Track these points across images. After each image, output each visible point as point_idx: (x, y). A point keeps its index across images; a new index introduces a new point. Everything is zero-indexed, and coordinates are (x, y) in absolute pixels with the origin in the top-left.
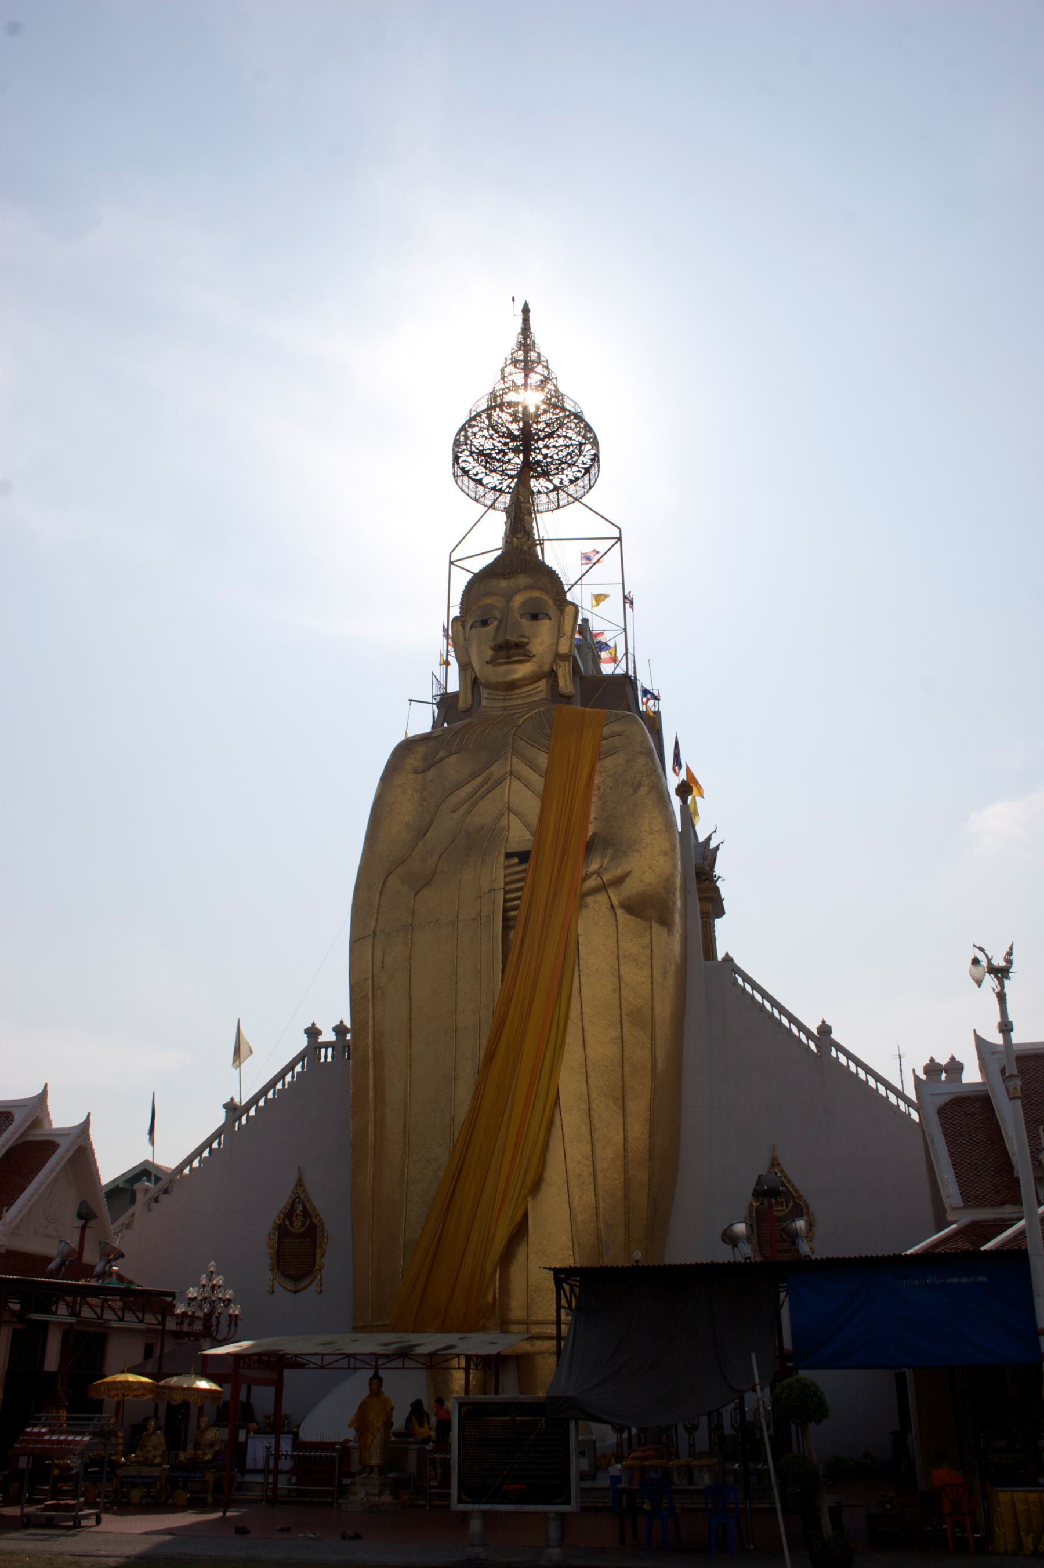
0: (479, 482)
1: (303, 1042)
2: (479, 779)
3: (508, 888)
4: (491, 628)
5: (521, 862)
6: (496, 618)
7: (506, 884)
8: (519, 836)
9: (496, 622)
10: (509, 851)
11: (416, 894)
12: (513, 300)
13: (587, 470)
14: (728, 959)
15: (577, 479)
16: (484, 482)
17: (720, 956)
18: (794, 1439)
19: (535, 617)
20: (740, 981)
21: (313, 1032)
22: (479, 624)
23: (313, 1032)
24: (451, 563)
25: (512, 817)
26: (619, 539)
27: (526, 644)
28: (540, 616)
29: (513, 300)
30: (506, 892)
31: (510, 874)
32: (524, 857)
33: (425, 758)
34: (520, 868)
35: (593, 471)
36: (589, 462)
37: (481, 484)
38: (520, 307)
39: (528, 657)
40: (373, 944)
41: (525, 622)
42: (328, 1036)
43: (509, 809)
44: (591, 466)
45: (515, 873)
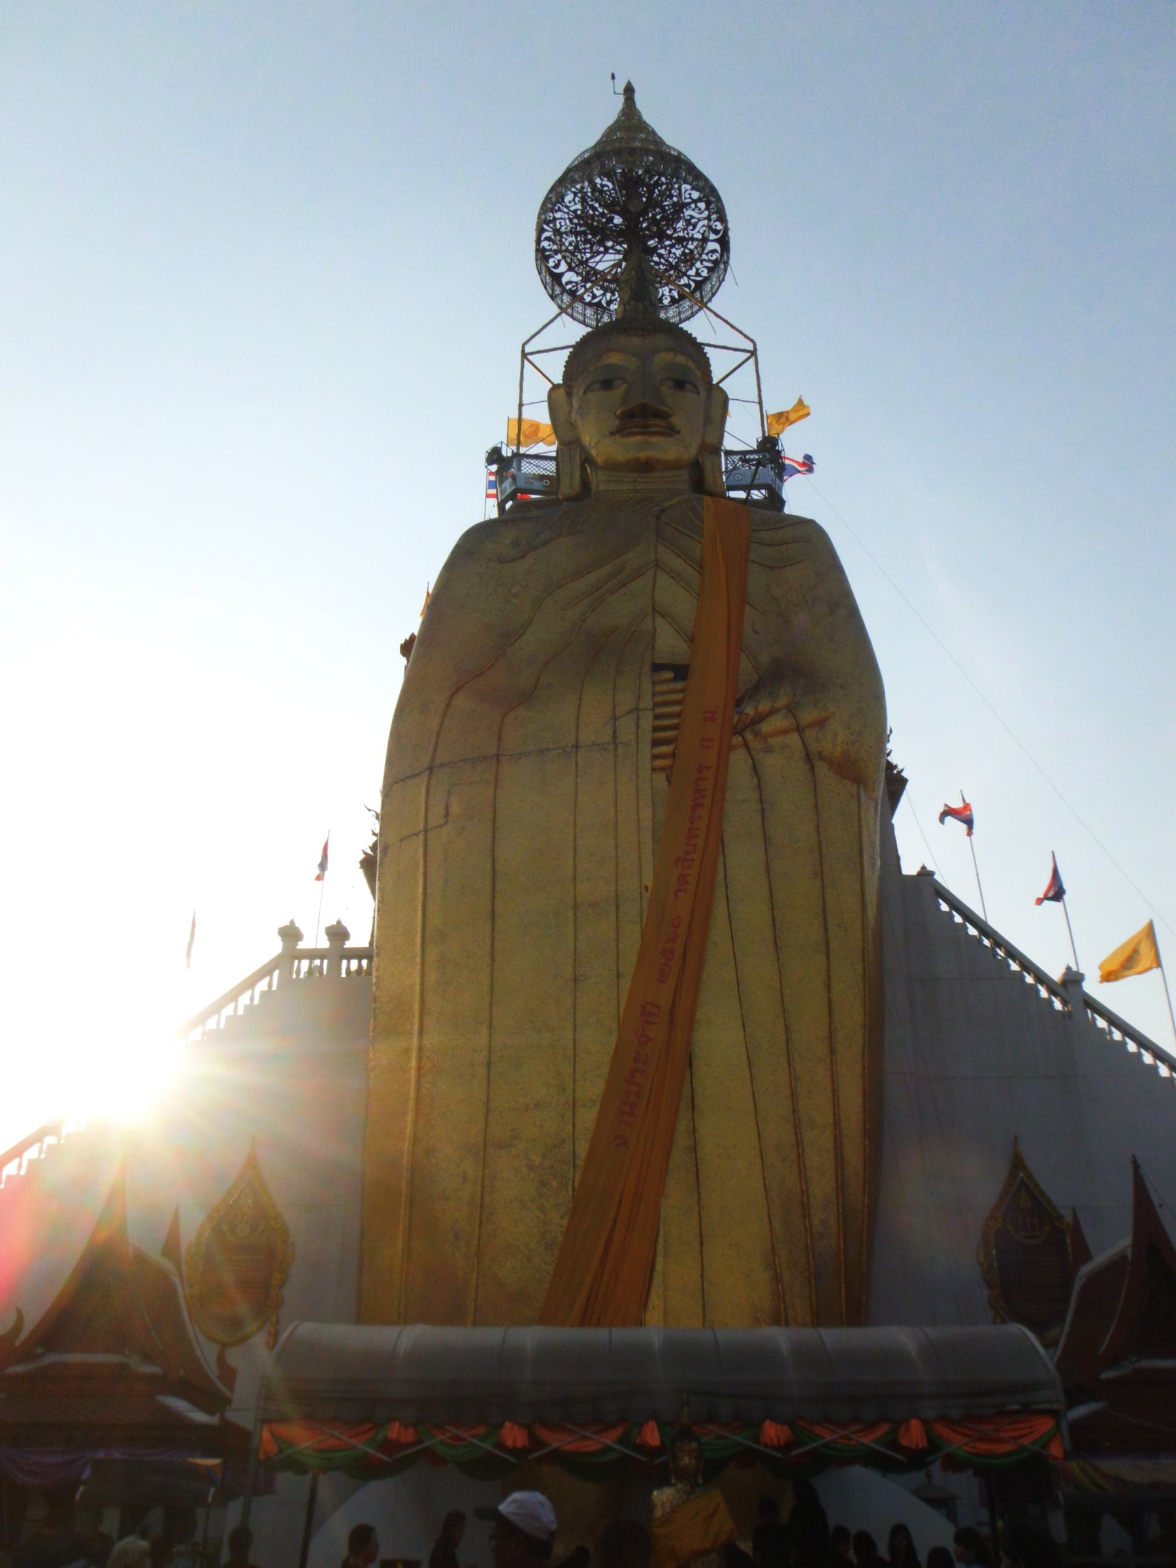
0: (557, 278)
1: (276, 947)
2: (607, 569)
3: (658, 711)
4: (620, 390)
5: (676, 679)
6: (624, 380)
7: (656, 705)
8: (669, 643)
9: (624, 386)
10: (658, 661)
11: (505, 715)
12: (613, 77)
13: (699, 285)
14: (925, 874)
15: (682, 297)
16: (564, 280)
17: (909, 868)
18: (406, 1452)
19: (680, 385)
20: (944, 907)
21: (290, 934)
22: (597, 386)
23: (290, 934)
24: (524, 355)
25: (659, 621)
26: (753, 353)
27: (670, 416)
28: (688, 386)
29: (613, 77)
30: (656, 717)
31: (662, 693)
32: (681, 672)
33: (516, 543)
34: (671, 686)
35: (707, 287)
36: (705, 273)
37: (560, 284)
38: (620, 88)
39: (672, 431)
40: (428, 792)
41: (667, 391)
42: (315, 939)
43: (654, 610)
44: (706, 279)
45: (670, 692)
